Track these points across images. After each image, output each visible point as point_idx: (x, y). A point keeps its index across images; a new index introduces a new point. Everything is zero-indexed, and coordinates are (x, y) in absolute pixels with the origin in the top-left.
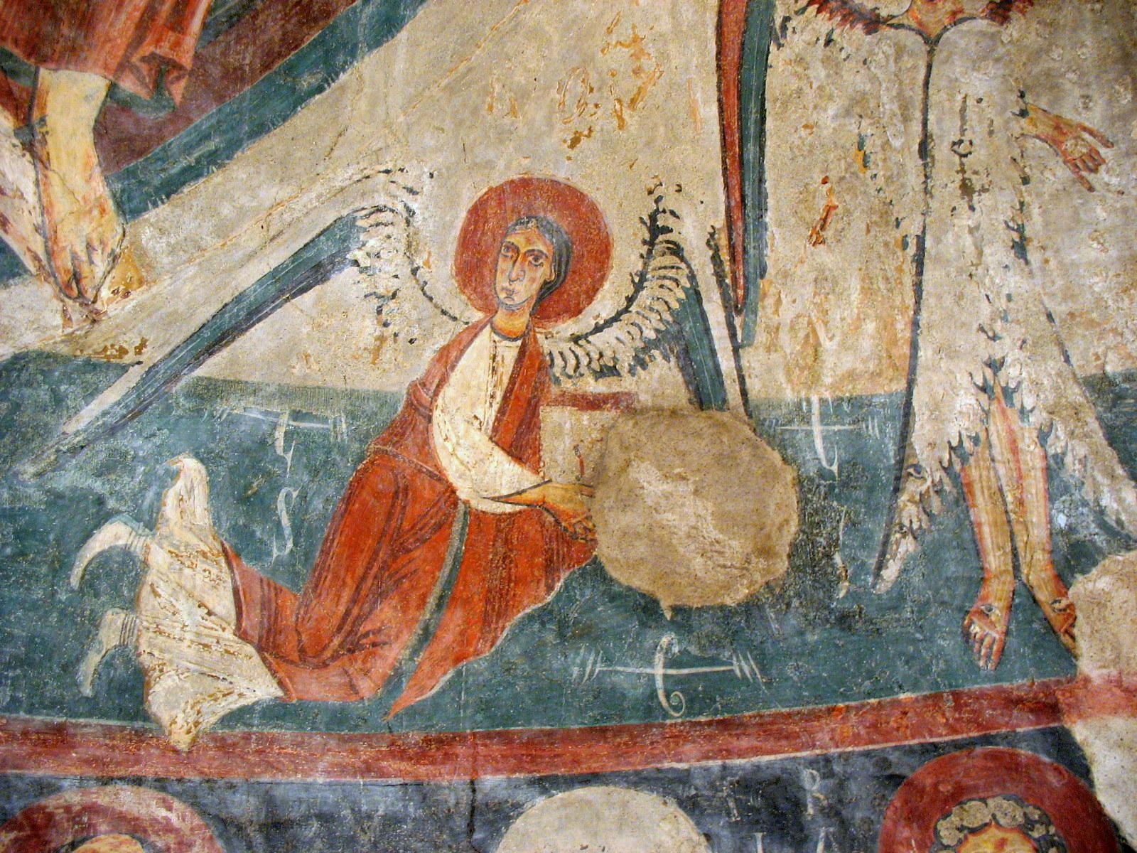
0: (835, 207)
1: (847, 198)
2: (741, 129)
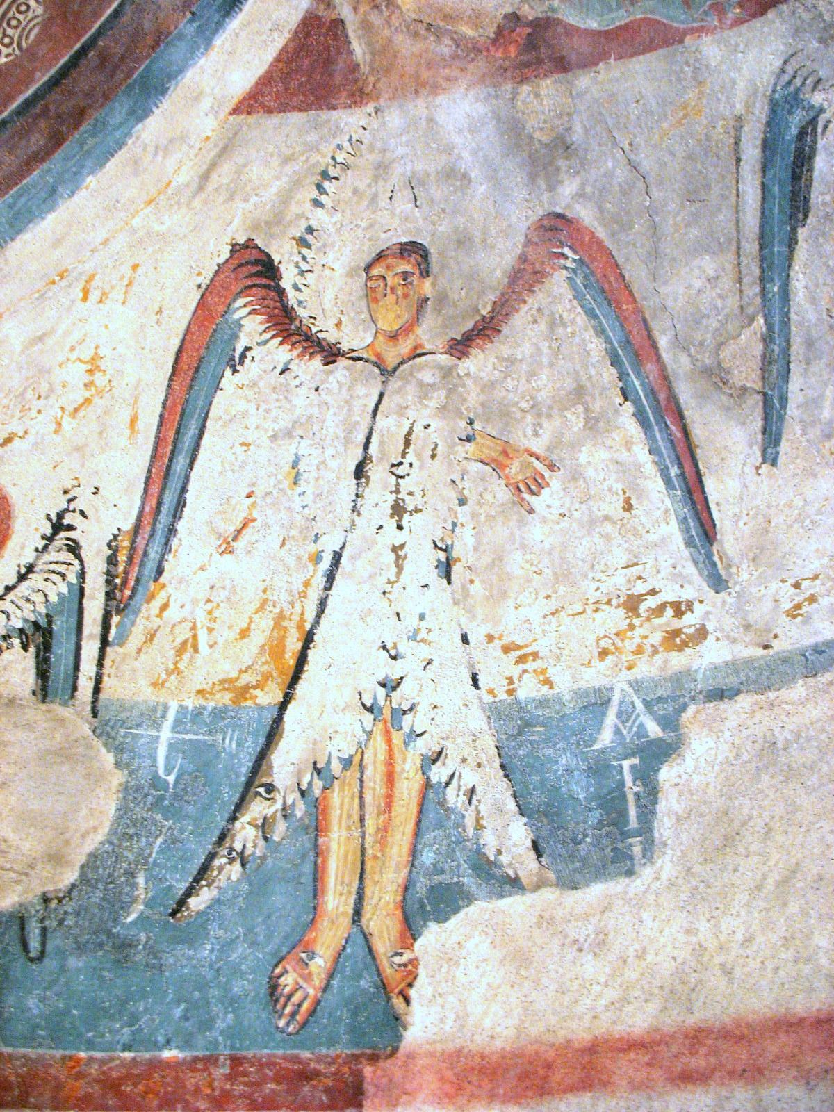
0: (254, 520)
1: (269, 512)
2: (175, 442)
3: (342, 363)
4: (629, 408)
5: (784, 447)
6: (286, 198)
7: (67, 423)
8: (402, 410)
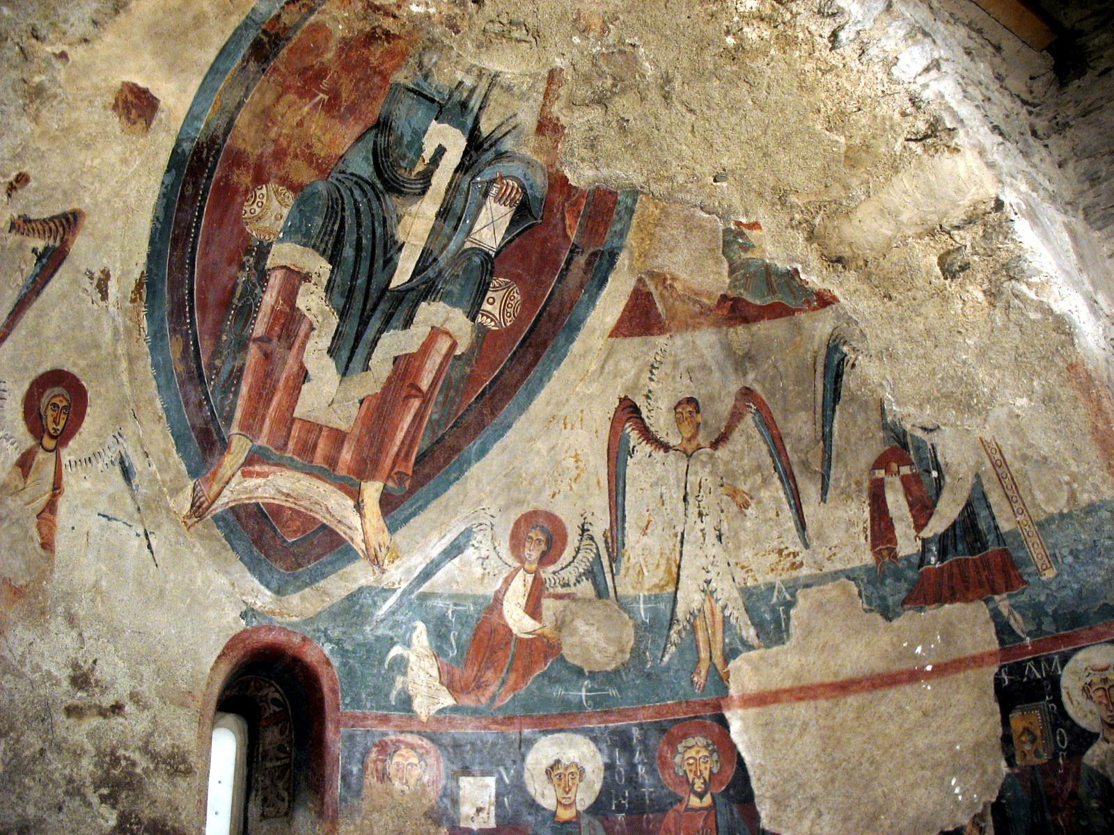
3: (671, 452)
4: (776, 475)
5: (828, 496)
6: (638, 376)
7: (574, 485)
8: (696, 473)
